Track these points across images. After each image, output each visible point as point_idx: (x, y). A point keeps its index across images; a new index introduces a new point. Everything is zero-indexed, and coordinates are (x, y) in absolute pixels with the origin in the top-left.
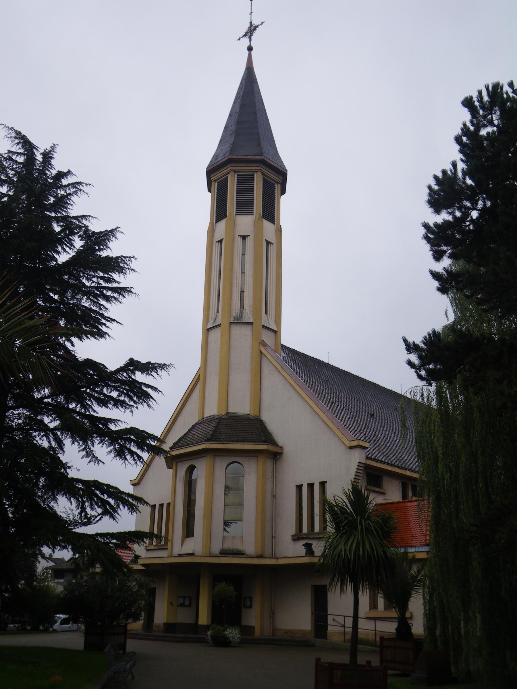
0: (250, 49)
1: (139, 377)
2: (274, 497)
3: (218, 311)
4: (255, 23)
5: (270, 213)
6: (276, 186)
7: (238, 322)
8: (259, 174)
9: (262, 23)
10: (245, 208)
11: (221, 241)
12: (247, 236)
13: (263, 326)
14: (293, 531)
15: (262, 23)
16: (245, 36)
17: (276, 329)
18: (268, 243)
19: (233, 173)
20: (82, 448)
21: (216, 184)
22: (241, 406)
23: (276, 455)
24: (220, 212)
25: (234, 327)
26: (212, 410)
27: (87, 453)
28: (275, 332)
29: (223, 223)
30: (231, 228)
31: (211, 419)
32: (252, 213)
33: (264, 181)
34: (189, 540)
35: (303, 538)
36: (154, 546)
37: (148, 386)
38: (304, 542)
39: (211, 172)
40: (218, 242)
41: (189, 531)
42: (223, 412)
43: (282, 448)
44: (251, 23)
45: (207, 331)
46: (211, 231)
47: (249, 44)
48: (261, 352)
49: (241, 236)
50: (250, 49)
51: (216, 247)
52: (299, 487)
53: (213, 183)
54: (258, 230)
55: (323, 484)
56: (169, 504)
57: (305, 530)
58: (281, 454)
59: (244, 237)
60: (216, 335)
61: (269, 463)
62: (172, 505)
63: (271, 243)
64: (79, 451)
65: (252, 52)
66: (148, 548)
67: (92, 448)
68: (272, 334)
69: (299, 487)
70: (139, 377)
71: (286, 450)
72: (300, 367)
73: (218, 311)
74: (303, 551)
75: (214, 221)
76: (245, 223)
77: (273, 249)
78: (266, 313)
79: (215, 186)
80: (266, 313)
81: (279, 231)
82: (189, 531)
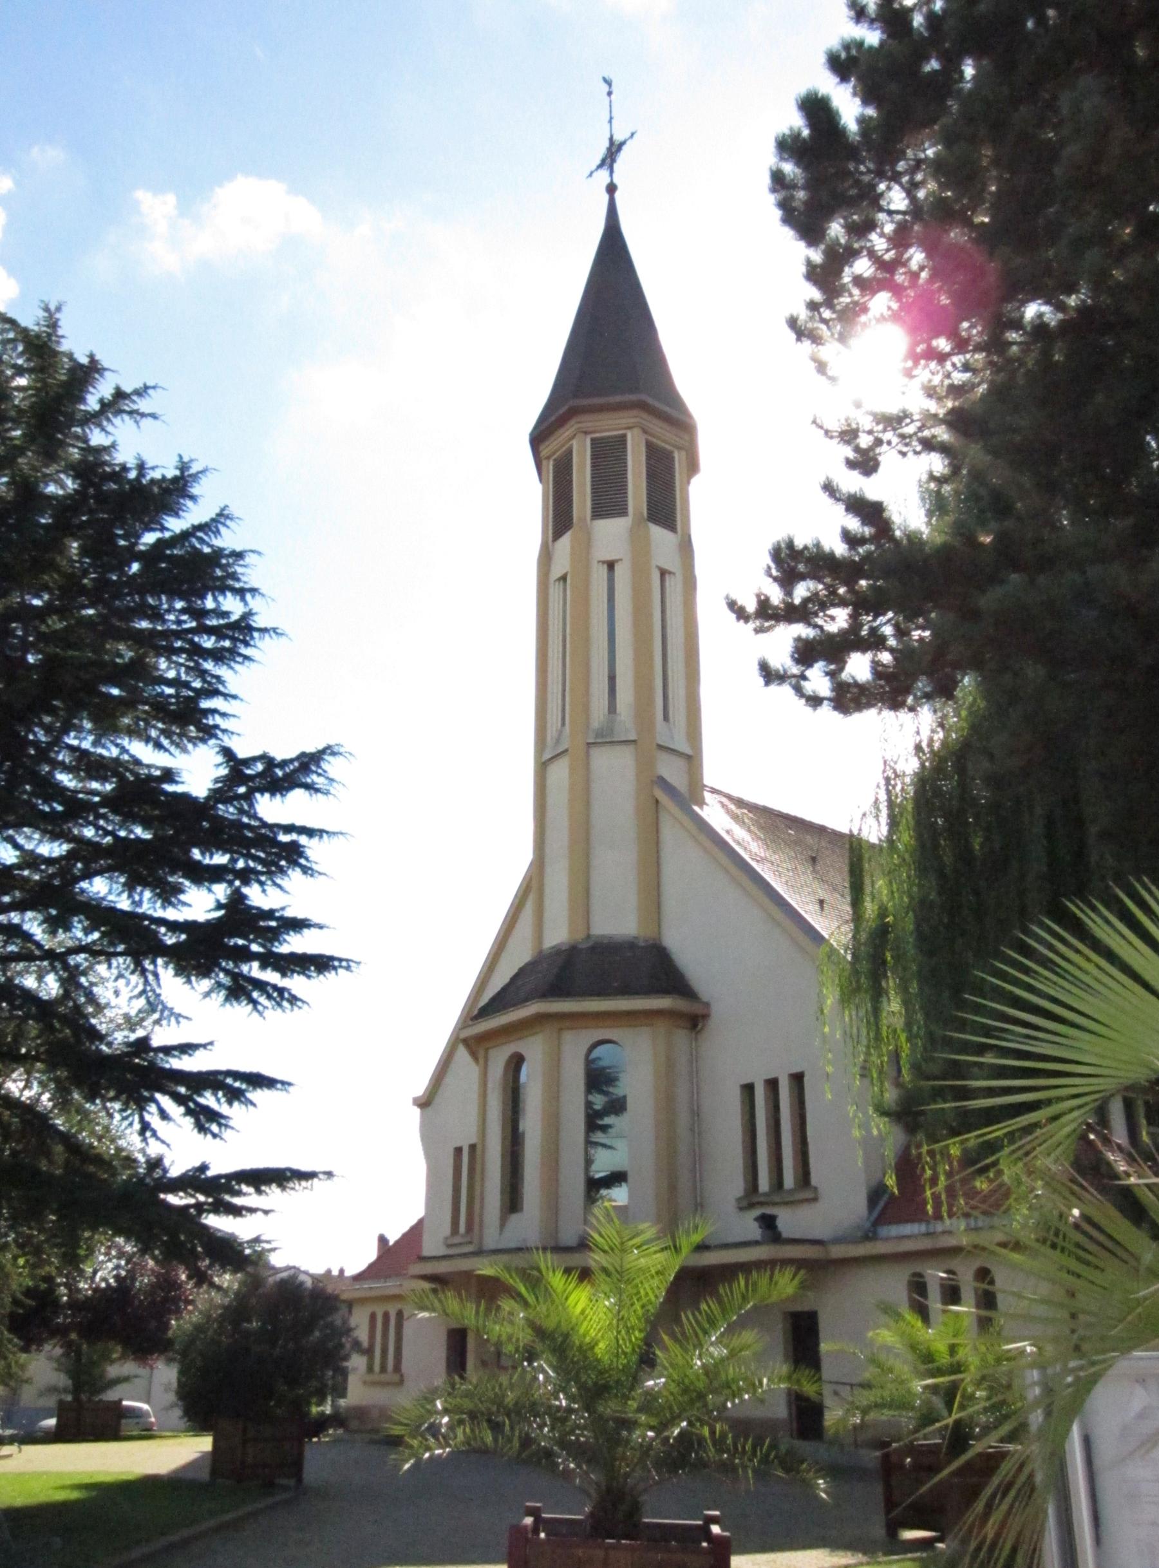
0: (611, 189)
1: (270, 809)
2: (696, 1113)
3: (563, 724)
4: (618, 138)
5: (665, 509)
6: (676, 455)
7: (605, 738)
8: (636, 431)
9: (632, 134)
10: (609, 503)
11: (564, 578)
12: (617, 561)
13: (661, 747)
14: (736, 1186)
15: (632, 134)
16: (600, 166)
17: (688, 751)
18: (663, 573)
19: (582, 435)
20: (136, 992)
21: (551, 463)
22: (618, 920)
23: (695, 1021)
24: (560, 518)
25: (596, 752)
26: (558, 935)
27: (149, 1002)
28: (689, 758)
29: (566, 540)
30: (584, 549)
31: (557, 952)
32: (623, 512)
33: (650, 447)
34: (514, 1218)
35: (761, 1204)
36: (462, 1236)
37: (289, 829)
38: (757, 1212)
39: (538, 439)
40: (559, 580)
41: (513, 1201)
42: (580, 936)
43: (707, 1005)
44: (611, 139)
45: (542, 768)
46: (546, 558)
47: (608, 180)
48: (657, 801)
49: (604, 562)
50: (611, 189)
51: (555, 591)
52: (749, 1089)
53: (544, 462)
54: (640, 548)
55: (798, 1079)
56: (473, 1147)
57: (764, 1184)
58: (705, 1017)
59: (611, 565)
60: (560, 773)
61: (681, 1037)
62: (479, 1148)
63: (670, 573)
64: (131, 998)
65: (617, 195)
66: (450, 1242)
67: (158, 991)
68: (680, 763)
69: (749, 1089)
70: (270, 809)
71: (717, 1010)
72: (750, 831)
73: (563, 724)
74: (754, 1231)
75: (550, 539)
76: (611, 535)
77: (674, 586)
78: (666, 718)
79: (550, 466)
80: (666, 718)
81: (686, 548)
82: (513, 1201)
